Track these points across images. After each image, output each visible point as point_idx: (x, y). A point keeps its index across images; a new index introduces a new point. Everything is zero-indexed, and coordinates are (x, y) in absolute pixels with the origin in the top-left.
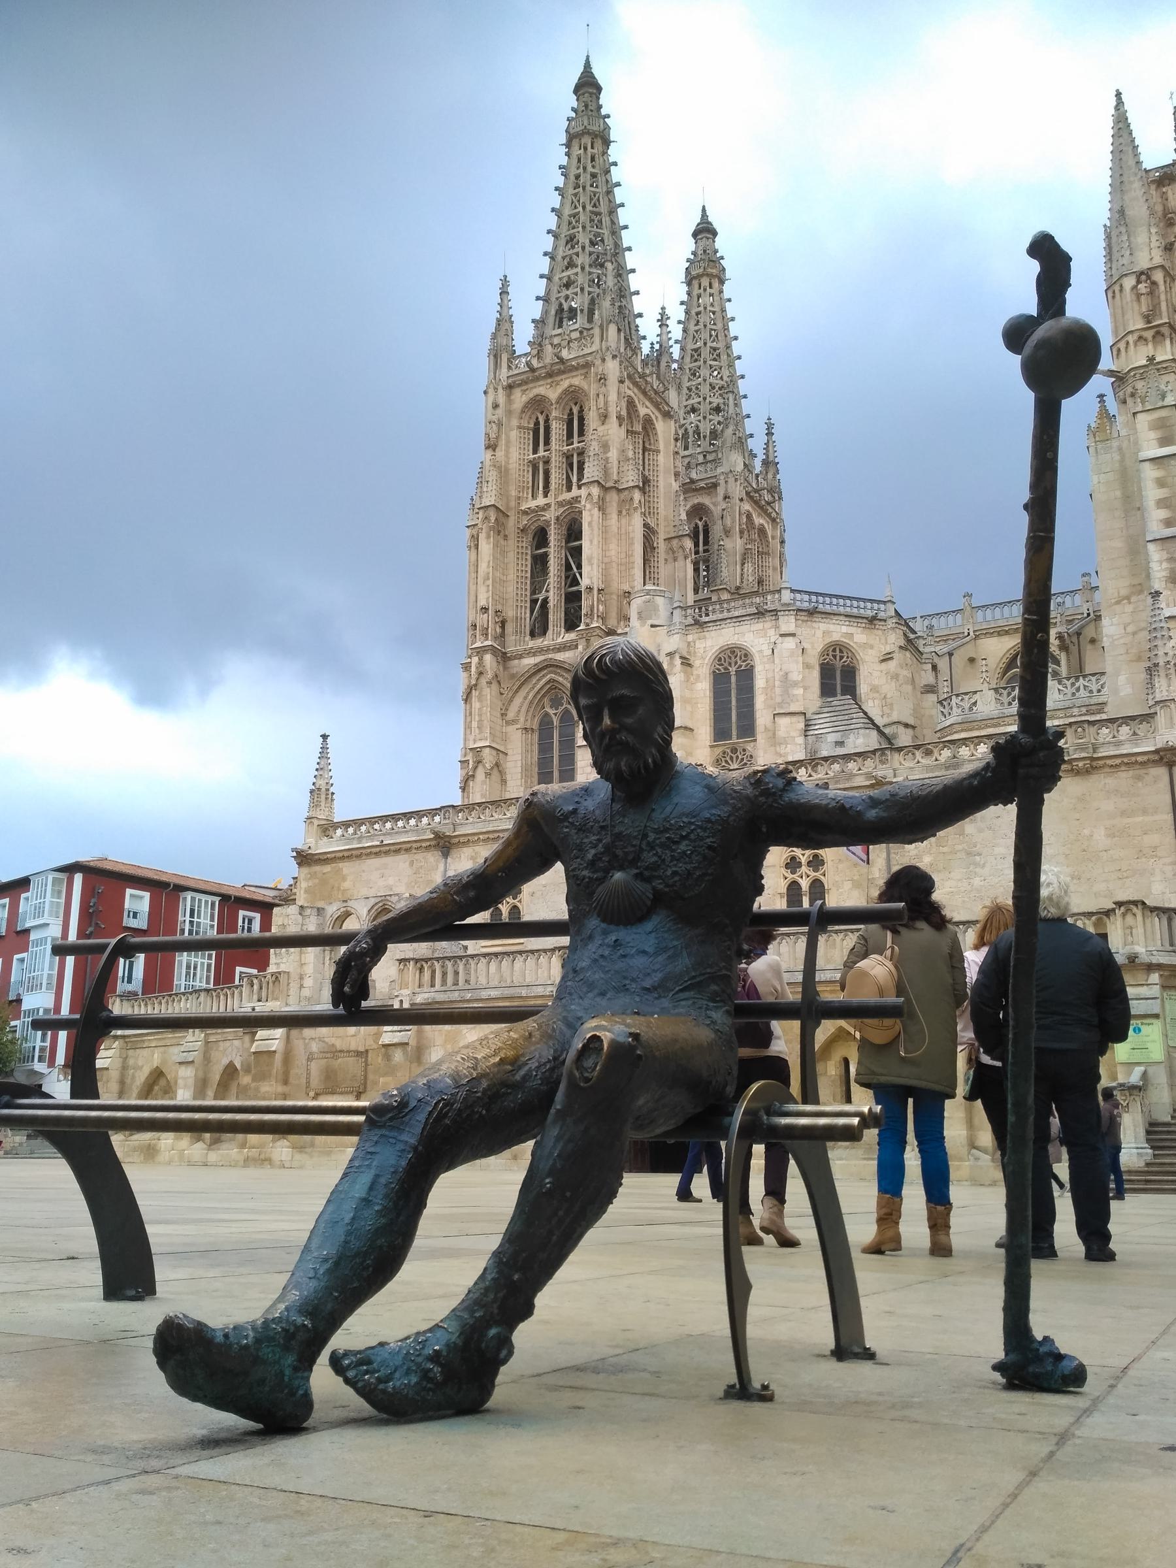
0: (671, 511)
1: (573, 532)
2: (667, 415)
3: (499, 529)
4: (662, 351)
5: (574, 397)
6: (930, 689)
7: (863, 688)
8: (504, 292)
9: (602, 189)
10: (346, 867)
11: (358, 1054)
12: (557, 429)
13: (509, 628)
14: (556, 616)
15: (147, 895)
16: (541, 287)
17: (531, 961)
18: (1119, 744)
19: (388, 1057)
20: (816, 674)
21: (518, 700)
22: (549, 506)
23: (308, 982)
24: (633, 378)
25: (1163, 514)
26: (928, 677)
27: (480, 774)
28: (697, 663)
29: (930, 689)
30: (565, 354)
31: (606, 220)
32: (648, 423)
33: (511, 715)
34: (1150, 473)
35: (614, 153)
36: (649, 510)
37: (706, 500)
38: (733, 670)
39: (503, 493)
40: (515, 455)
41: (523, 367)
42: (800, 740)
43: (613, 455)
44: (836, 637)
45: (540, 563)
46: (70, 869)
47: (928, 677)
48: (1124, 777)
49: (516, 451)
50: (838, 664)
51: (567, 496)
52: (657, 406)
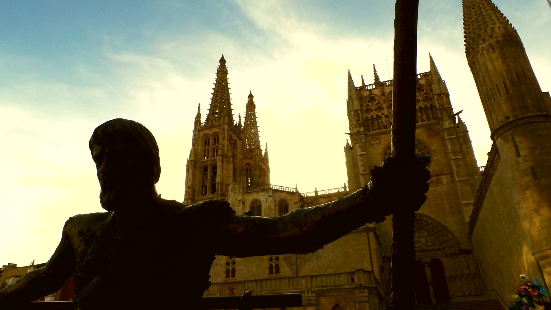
1: (215, 168)
13: (196, 193)
20: (278, 207)
28: (246, 203)
30: (214, 123)
32: (235, 141)
34: (359, 158)
35: (228, 76)
38: (256, 205)
40: (200, 148)
43: (226, 149)
44: (283, 197)
49: (200, 147)
51: (213, 159)
52: (238, 137)
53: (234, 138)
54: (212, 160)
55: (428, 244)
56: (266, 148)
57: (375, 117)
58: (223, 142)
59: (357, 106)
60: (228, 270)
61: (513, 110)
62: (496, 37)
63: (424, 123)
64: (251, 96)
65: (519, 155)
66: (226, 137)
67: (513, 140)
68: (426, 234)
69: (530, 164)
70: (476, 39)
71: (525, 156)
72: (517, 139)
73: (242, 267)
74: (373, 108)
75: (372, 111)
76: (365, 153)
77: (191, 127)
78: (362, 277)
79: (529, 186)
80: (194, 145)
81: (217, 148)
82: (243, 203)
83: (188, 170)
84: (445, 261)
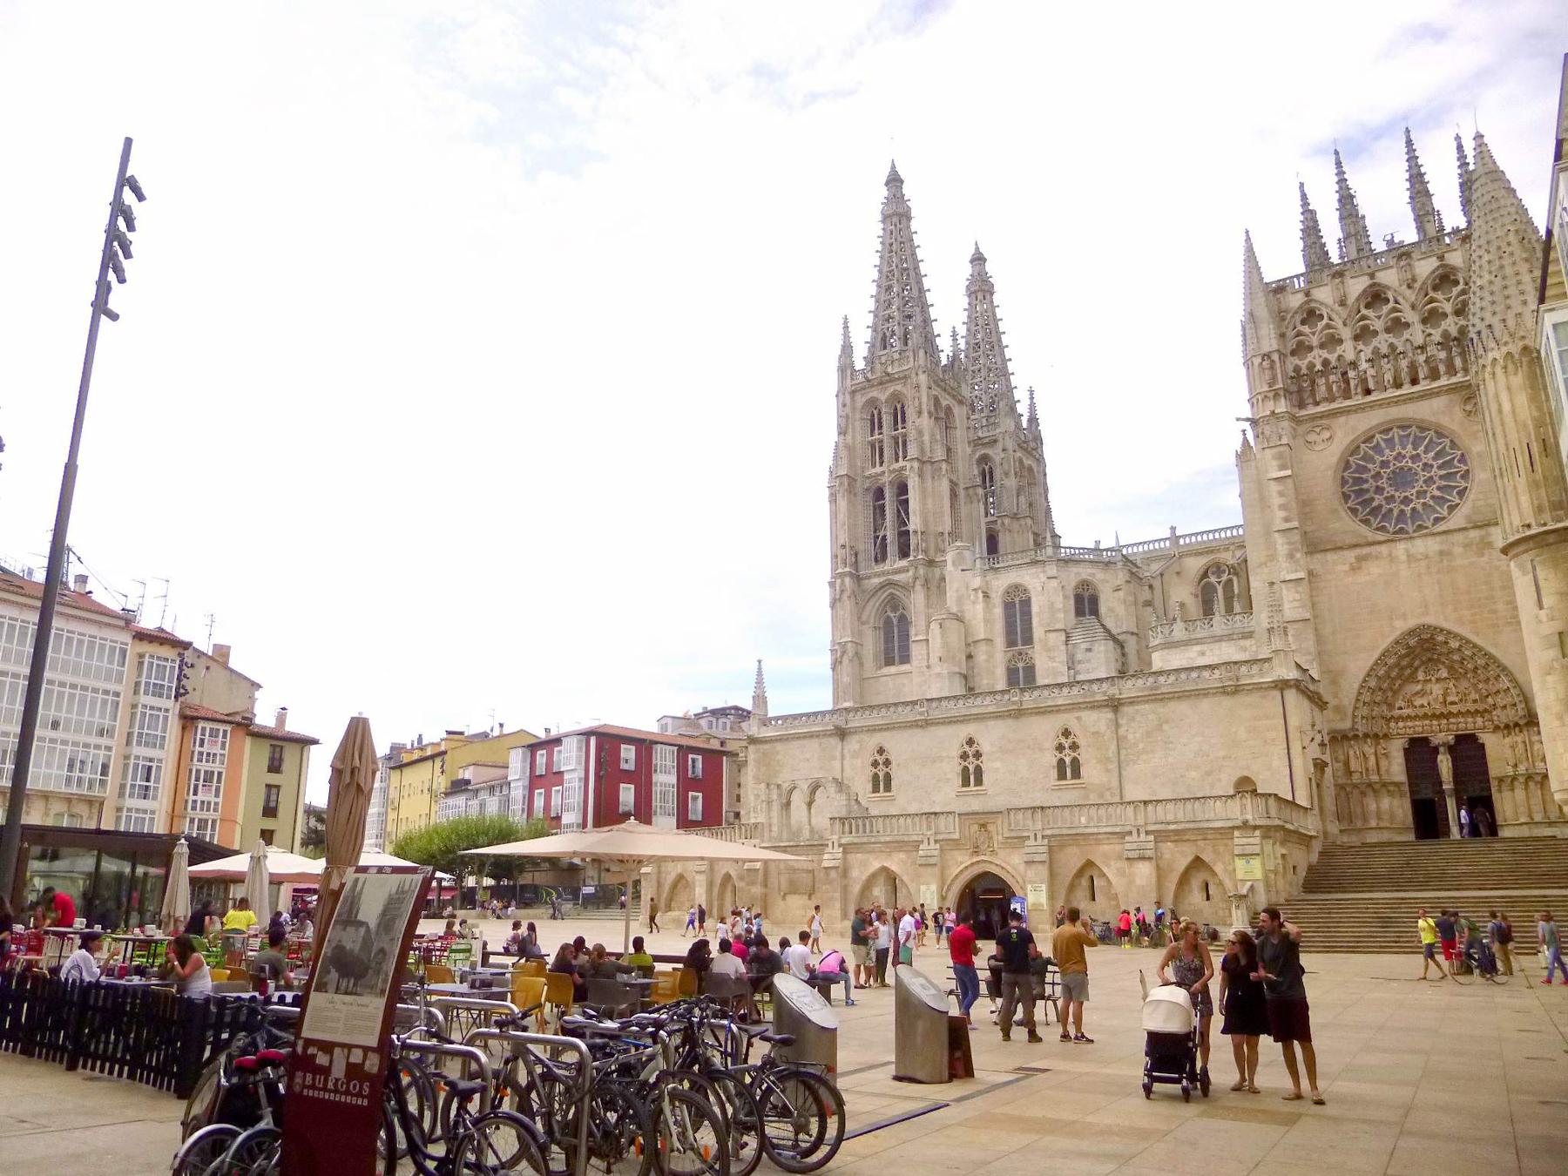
0: (967, 470)
1: (903, 489)
2: (961, 402)
3: (851, 490)
4: (955, 358)
5: (897, 398)
6: (1148, 603)
7: (1103, 610)
8: (846, 327)
9: (908, 252)
10: (779, 746)
11: (808, 871)
12: (887, 420)
13: (860, 558)
14: (892, 549)
15: (633, 748)
16: (870, 320)
17: (909, 820)
18: (1252, 676)
19: (827, 875)
20: (1072, 602)
21: (868, 608)
22: (885, 472)
23: (775, 829)
24: (937, 382)
25: (1282, 514)
26: (1145, 594)
27: (846, 660)
28: (993, 595)
29: (1148, 603)
30: (889, 370)
31: (912, 273)
32: (949, 409)
33: (864, 618)
34: (1274, 487)
35: (914, 225)
36: (953, 470)
37: (990, 451)
38: (1017, 600)
39: (852, 466)
40: (859, 438)
41: (861, 378)
42: (1063, 648)
43: (926, 438)
44: (1084, 576)
45: (880, 511)
46: (587, 734)
47: (1145, 594)
48: (1254, 698)
49: (860, 435)
50: (1087, 594)
51: (896, 466)
52: (954, 397)
53: (944, 403)
54: (894, 471)
55: (1449, 699)
56: (1032, 407)
57: (1319, 367)
58: (918, 421)
59: (1270, 343)
60: (966, 769)
61: (1539, 510)
62: (1523, 337)
63: (1454, 380)
64: (978, 259)
65: (1541, 608)
66: (924, 407)
67: (1534, 568)
68: (1445, 675)
69: (1558, 626)
70: (1484, 335)
71: (1551, 608)
72: (1541, 574)
73: (998, 764)
74: (1315, 341)
75: (1311, 349)
76: (1288, 472)
77: (830, 381)
78: (1249, 806)
79: (1552, 668)
80: (842, 432)
81: (905, 435)
82: (986, 596)
83: (833, 499)
84: (1490, 741)
